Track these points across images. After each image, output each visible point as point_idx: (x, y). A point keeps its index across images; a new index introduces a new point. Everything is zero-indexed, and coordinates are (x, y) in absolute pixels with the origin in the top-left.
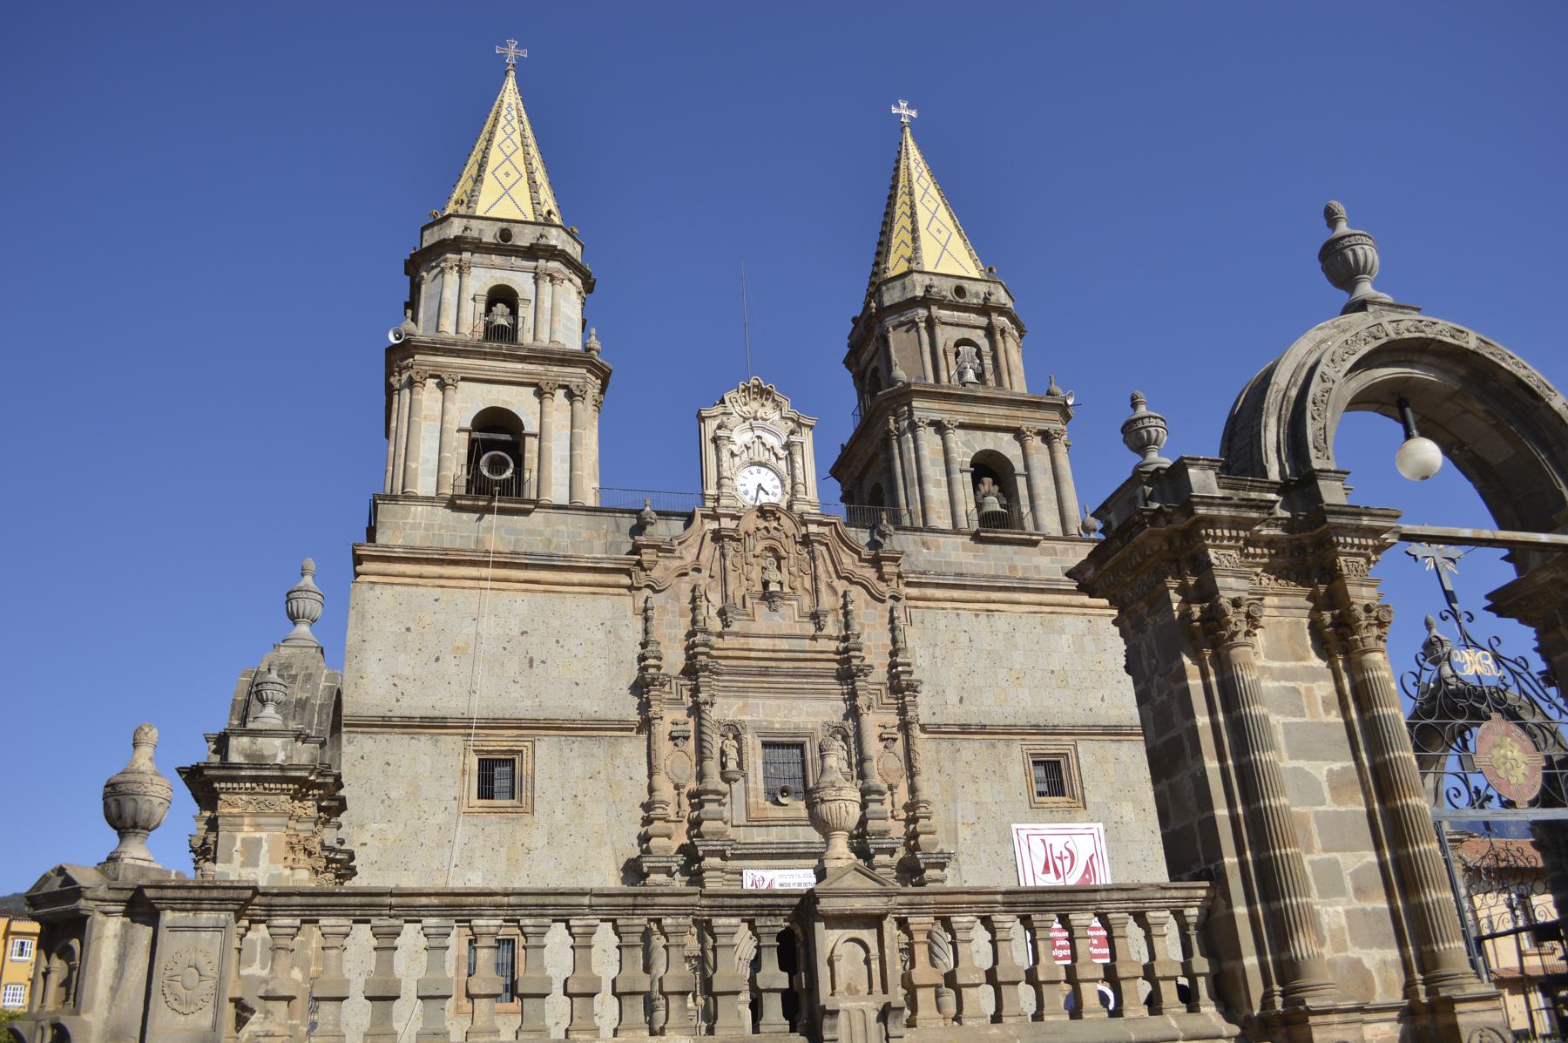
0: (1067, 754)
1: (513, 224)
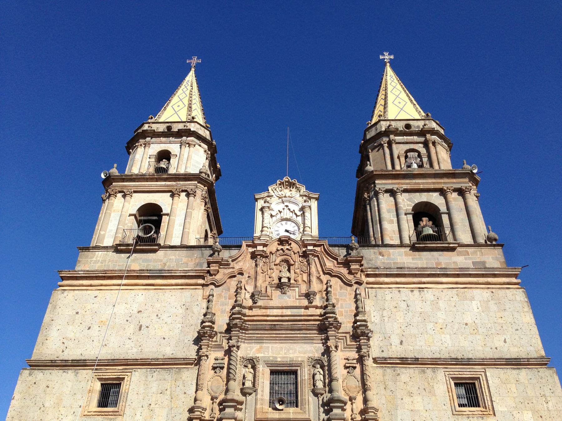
0: (479, 378)
1: (173, 124)
